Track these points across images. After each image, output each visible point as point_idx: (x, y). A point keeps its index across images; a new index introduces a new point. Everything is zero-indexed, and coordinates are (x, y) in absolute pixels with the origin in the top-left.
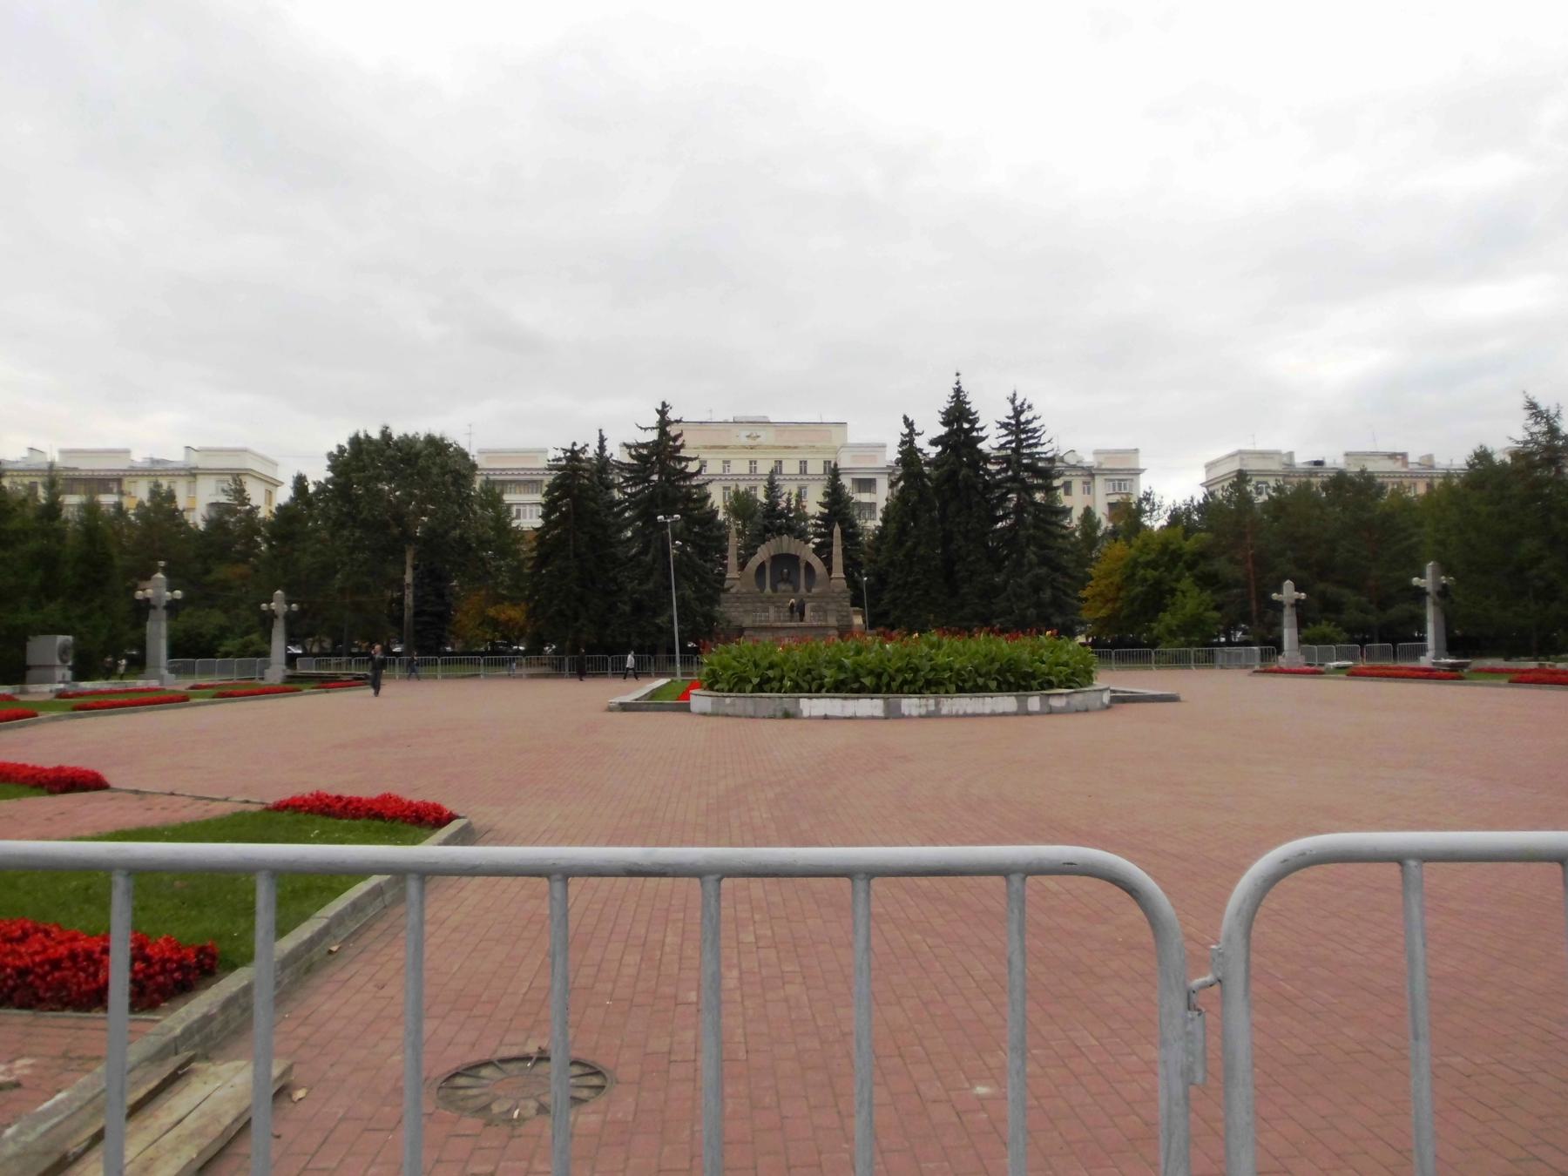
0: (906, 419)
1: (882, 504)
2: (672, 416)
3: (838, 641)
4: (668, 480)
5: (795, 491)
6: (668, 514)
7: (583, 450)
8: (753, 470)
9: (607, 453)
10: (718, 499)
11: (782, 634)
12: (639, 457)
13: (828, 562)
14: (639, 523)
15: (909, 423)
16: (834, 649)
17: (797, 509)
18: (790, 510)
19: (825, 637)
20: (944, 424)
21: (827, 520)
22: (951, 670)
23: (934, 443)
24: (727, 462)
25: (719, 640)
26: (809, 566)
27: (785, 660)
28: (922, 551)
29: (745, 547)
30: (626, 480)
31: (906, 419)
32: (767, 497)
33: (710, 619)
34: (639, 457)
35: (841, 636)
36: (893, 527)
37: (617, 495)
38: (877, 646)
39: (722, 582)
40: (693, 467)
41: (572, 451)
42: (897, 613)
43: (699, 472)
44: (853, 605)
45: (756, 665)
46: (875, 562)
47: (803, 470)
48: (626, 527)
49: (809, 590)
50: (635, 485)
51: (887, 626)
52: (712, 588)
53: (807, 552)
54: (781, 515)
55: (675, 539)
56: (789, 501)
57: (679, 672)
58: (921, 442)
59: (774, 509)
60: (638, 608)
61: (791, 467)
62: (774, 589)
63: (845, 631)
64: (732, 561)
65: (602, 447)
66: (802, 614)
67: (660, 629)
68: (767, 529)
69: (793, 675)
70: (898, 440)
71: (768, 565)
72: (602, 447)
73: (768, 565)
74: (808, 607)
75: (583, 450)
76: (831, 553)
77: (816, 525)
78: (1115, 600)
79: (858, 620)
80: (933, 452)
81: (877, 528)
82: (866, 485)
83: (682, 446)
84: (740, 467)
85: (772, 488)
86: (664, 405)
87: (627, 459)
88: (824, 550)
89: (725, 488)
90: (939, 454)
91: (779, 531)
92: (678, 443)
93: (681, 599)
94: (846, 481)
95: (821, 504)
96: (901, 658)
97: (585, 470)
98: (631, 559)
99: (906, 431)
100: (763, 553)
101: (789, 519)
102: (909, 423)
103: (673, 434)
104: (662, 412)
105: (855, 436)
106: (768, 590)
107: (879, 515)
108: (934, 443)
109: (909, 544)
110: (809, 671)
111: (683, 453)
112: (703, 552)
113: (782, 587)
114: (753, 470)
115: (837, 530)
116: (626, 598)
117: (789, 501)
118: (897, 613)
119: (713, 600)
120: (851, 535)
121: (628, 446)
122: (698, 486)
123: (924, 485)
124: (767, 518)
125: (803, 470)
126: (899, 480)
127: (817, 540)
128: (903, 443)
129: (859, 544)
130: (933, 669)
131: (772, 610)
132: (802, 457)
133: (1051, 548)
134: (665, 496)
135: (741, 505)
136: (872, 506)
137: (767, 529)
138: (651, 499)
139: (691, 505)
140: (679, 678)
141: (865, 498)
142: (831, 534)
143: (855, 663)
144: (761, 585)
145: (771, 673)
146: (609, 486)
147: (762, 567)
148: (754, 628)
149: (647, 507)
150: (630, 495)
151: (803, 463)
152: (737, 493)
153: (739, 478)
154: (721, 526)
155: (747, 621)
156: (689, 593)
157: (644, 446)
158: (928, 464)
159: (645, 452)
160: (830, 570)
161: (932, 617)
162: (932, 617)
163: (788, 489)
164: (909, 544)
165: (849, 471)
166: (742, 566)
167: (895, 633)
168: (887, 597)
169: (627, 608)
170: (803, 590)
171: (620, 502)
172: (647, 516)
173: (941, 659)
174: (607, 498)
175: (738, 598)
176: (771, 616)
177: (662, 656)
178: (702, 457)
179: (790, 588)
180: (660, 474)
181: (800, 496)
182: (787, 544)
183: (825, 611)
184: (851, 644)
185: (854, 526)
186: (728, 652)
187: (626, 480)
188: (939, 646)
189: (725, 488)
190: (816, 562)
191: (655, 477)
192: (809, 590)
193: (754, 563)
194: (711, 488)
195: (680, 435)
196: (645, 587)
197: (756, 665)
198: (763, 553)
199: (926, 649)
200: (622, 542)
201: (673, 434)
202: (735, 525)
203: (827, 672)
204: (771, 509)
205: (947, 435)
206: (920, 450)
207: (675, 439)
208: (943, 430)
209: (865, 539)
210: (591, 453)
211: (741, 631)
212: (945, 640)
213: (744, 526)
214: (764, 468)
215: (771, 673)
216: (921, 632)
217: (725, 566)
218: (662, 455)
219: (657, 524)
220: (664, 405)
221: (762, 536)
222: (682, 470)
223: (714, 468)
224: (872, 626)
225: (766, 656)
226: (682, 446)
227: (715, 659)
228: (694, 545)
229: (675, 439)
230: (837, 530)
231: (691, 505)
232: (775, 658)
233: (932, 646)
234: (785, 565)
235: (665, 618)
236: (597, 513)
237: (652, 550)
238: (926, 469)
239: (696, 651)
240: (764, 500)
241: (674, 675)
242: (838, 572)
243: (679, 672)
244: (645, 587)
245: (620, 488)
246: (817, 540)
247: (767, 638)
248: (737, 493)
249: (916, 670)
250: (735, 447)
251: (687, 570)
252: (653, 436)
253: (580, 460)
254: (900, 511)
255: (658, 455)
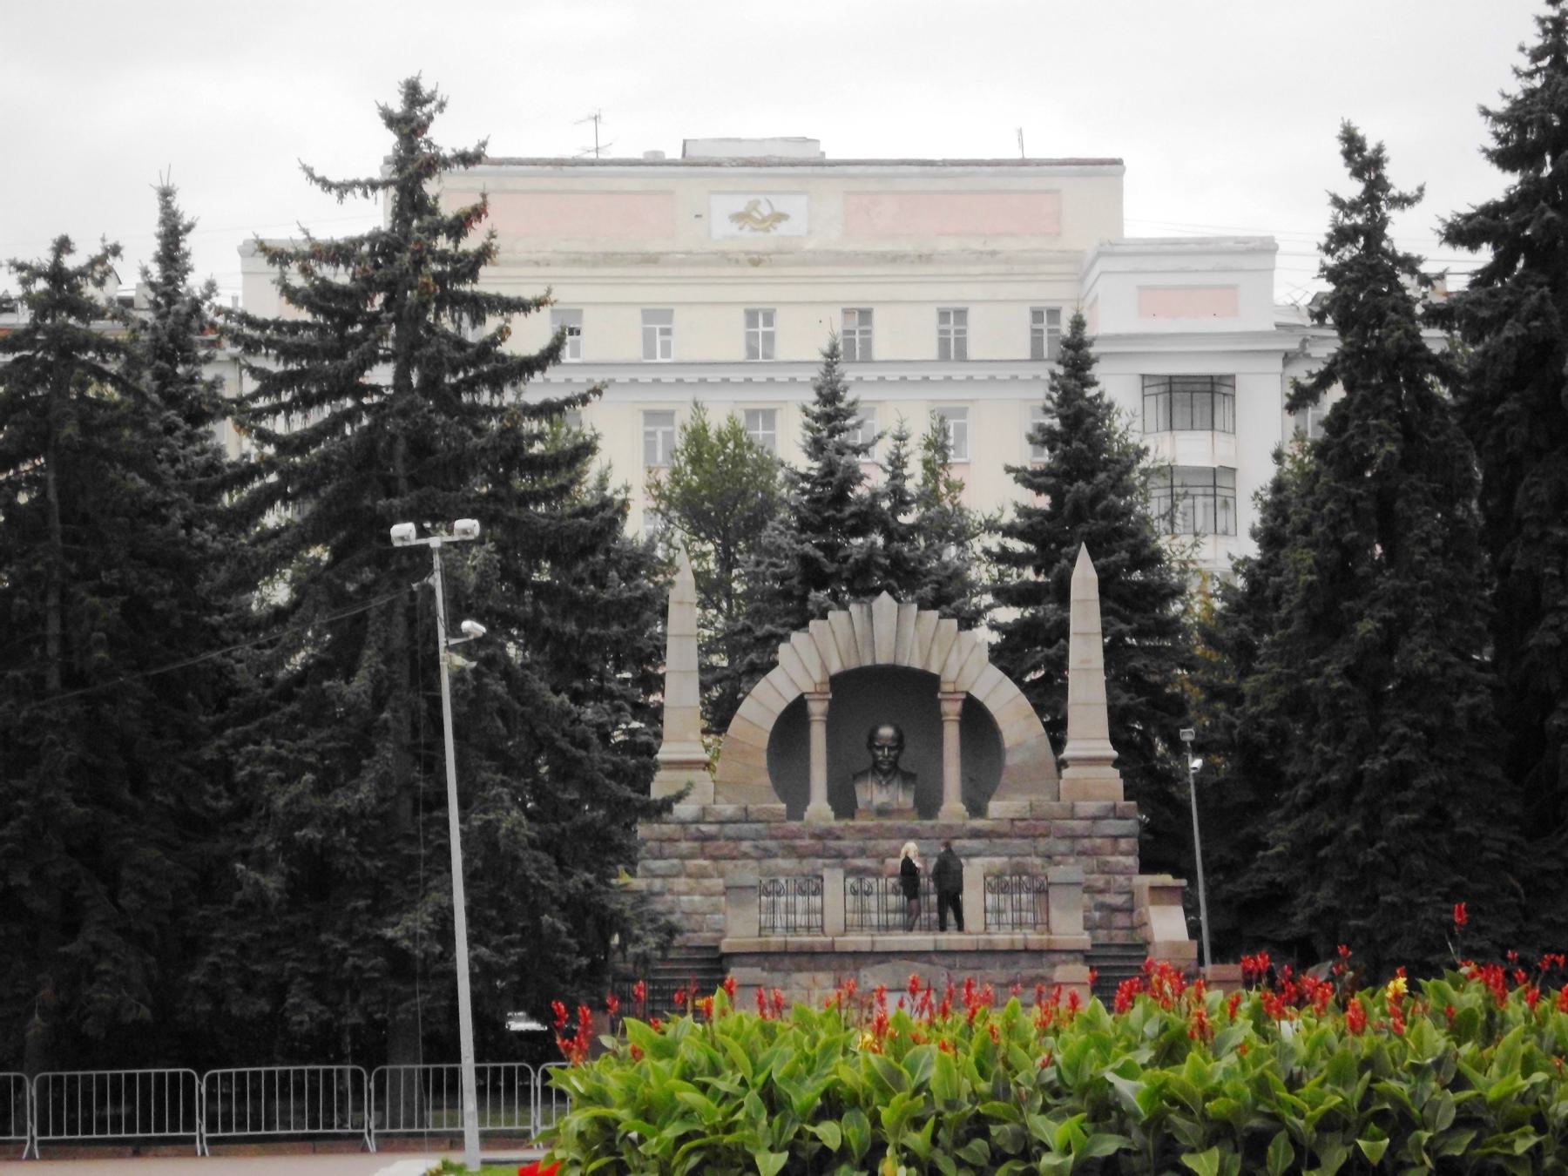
0: (1352, 144)
1: (1258, 474)
2: (444, 136)
3: (1091, 1004)
4: (431, 385)
5: (920, 428)
6: (431, 514)
7: (100, 267)
8: (759, 348)
9: (194, 283)
10: (628, 464)
11: (872, 978)
12: (320, 297)
13: (1049, 699)
14: (320, 553)
15: (1361, 158)
16: (1074, 1037)
17: (929, 497)
18: (901, 502)
19: (1044, 990)
20: (1504, 159)
21: (1047, 538)
22: (1540, 1124)
23: (1462, 233)
24: (658, 318)
25: (629, 1005)
26: (976, 717)
27: (887, 1084)
28: (1417, 654)
29: (731, 642)
30: (271, 384)
31: (1352, 144)
32: (817, 448)
33: (596, 920)
34: (320, 297)
35: (1102, 987)
36: (1302, 559)
37: (231, 442)
38: (1243, 1028)
39: (642, 777)
40: (526, 337)
41: (57, 275)
42: (1324, 895)
43: (551, 355)
44: (1147, 867)
45: (773, 1101)
46: (1234, 697)
47: (953, 348)
48: (269, 568)
49: (976, 808)
50: (306, 402)
51: (1284, 948)
52: (606, 798)
53: (966, 660)
54: (867, 519)
55: (460, 608)
56: (897, 464)
57: (471, 1126)
58: (1410, 233)
59: (840, 498)
60: (316, 878)
61: (903, 335)
62: (843, 803)
63: (1118, 970)
64: (681, 695)
65: (172, 255)
66: (951, 900)
67: (399, 962)
68: (813, 575)
69: (918, 1140)
70: (1322, 221)
71: (817, 709)
72: (172, 255)
73: (817, 709)
74: (974, 872)
75: (100, 267)
76: (1059, 665)
77: (1004, 557)
78: (1530, 75)
79: (1168, 926)
80: (1457, 269)
81: (1240, 565)
82: (1197, 395)
83: (484, 255)
84: (709, 335)
85: (831, 412)
86: (413, 93)
87: (272, 307)
88: (1032, 653)
89: (652, 416)
90: (1483, 279)
91: (861, 582)
92: (471, 243)
93: (481, 843)
94: (1115, 385)
95: (1027, 479)
96: (1340, 1077)
97: (105, 346)
98: (286, 693)
99: (1353, 189)
100: (804, 663)
101: (893, 533)
102: (1361, 158)
103: (448, 209)
104: (409, 120)
105: (1151, 211)
106: (819, 807)
107: (1250, 516)
108: (1462, 233)
109: (1366, 627)
110: (979, 1126)
111: (489, 282)
112: (568, 663)
113: (872, 794)
114: (759, 348)
115: (1084, 576)
116: (267, 842)
117: (897, 464)
118: (1324, 895)
119: (609, 849)
120: (1137, 597)
121: (278, 256)
122: (548, 410)
123: (1427, 400)
124: (829, 535)
125: (953, 348)
126: (1325, 380)
127: (1009, 614)
128: (1341, 236)
129: (1169, 627)
130: (1466, 1119)
131: (834, 881)
132: (951, 294)
133: (358, 1108)
134: (420, 447)
135: (718, 492)
136: (1218, 479)
137: (813, 575)
138: (368, 454)
139: (521, 483)
140: (472, 1154)
141: (1189, 449)
142: (1061, 592)
143: (1159, 1092)
144: (794, 792)
145: (829, 1133)
146: (203, 409)
147: (794, 718)
148: (766, 957)
149: (355, 490)
150: (287, 445)
151: (953, 318)
152: (697, 437)
153: (706, 375)
154: (639, 562)
155: (740, 928)
156: (511, 820)
157: (339, 253)
158: (1438, 316)
159: (341, 276)
160: (1057, 731)
161: (1459, 914)
162: (1459, 914)
163: (890, 422)
164: (1366, 627)
165: (1130, 346)
166: (720, 715)
167: (1319, 973)
168: (1280, 835)
169: (272, 883)
170: (953, 806)
171: (245, 473)
172: (351, 524)
173: (1498, 1083)
174: (192, 455)
175: (710, 841)
176: (836, 908)
177: (408, 1068)
178: (565, 295)
179: (902, 798)
180: (404, 360)
181: (938, 446)
182: (893, 630)
183: (1042, 891)
184: (1144, 1017)
185: (1149, 559)
186: (666, 1051)
187: (271, 384)
188: (1491, 1030)
189: (652, 416)
190: (1006, 701)
191: (381, 375)
192: (976, 808)
193: (762, 706)
194: (592, 419)
195: (478, 212)
196: (342, 800)
197: (773, 1101)
198: (804, 663)
199: (1436, 1040)
200: (249, 626)
201: (448, 209)
202: (686, 559)
203: (1054, 1131)
204: (832, 501)
205: (1513, 204)
206: (1410, 264)
207: (458, 227)
208: (1499, 184)
209: (1196, 606)
210: (131, 278)
211: (713, 966)
212: (1515, 1007)
213: (727, 562)
214: (803, 340)
215: (829, 1133)
216: (1420, 970)
217: (654, 716)
218: (159, 236)
219: (386, 554)
220: (413, 93)
221: (794, 599)
222: (486, 350)
223: (606, 340)
224: (1221, 952)
225: (810, 1064)
226: (484, 255)
227: (613, 1078)
228: (535, 636)
229: (458, 227)
230: (1084, 576)
231: (521, 483)
232: (850, 1074)
233: (1460, 1028)
234: (888, 702)
235: (418, 920)
236: (154, 513)
237: (370, 657)
238: (1434, 339)
239: (541, 1049)
240: (803, 463)
241: (456, 1141)
242: (1090, 730)
243: (471, 1126)
244: (342, 800)
245: (245, 415)
246: (1009, 614)
247: (812, 993)
248: (697, 437)
249: (1399, 1122)
250: (690, 259)
251: (504, 729)
252: (370, 216)
253: (87, 311)
254: (1339, 506)
255: (392, 288)
